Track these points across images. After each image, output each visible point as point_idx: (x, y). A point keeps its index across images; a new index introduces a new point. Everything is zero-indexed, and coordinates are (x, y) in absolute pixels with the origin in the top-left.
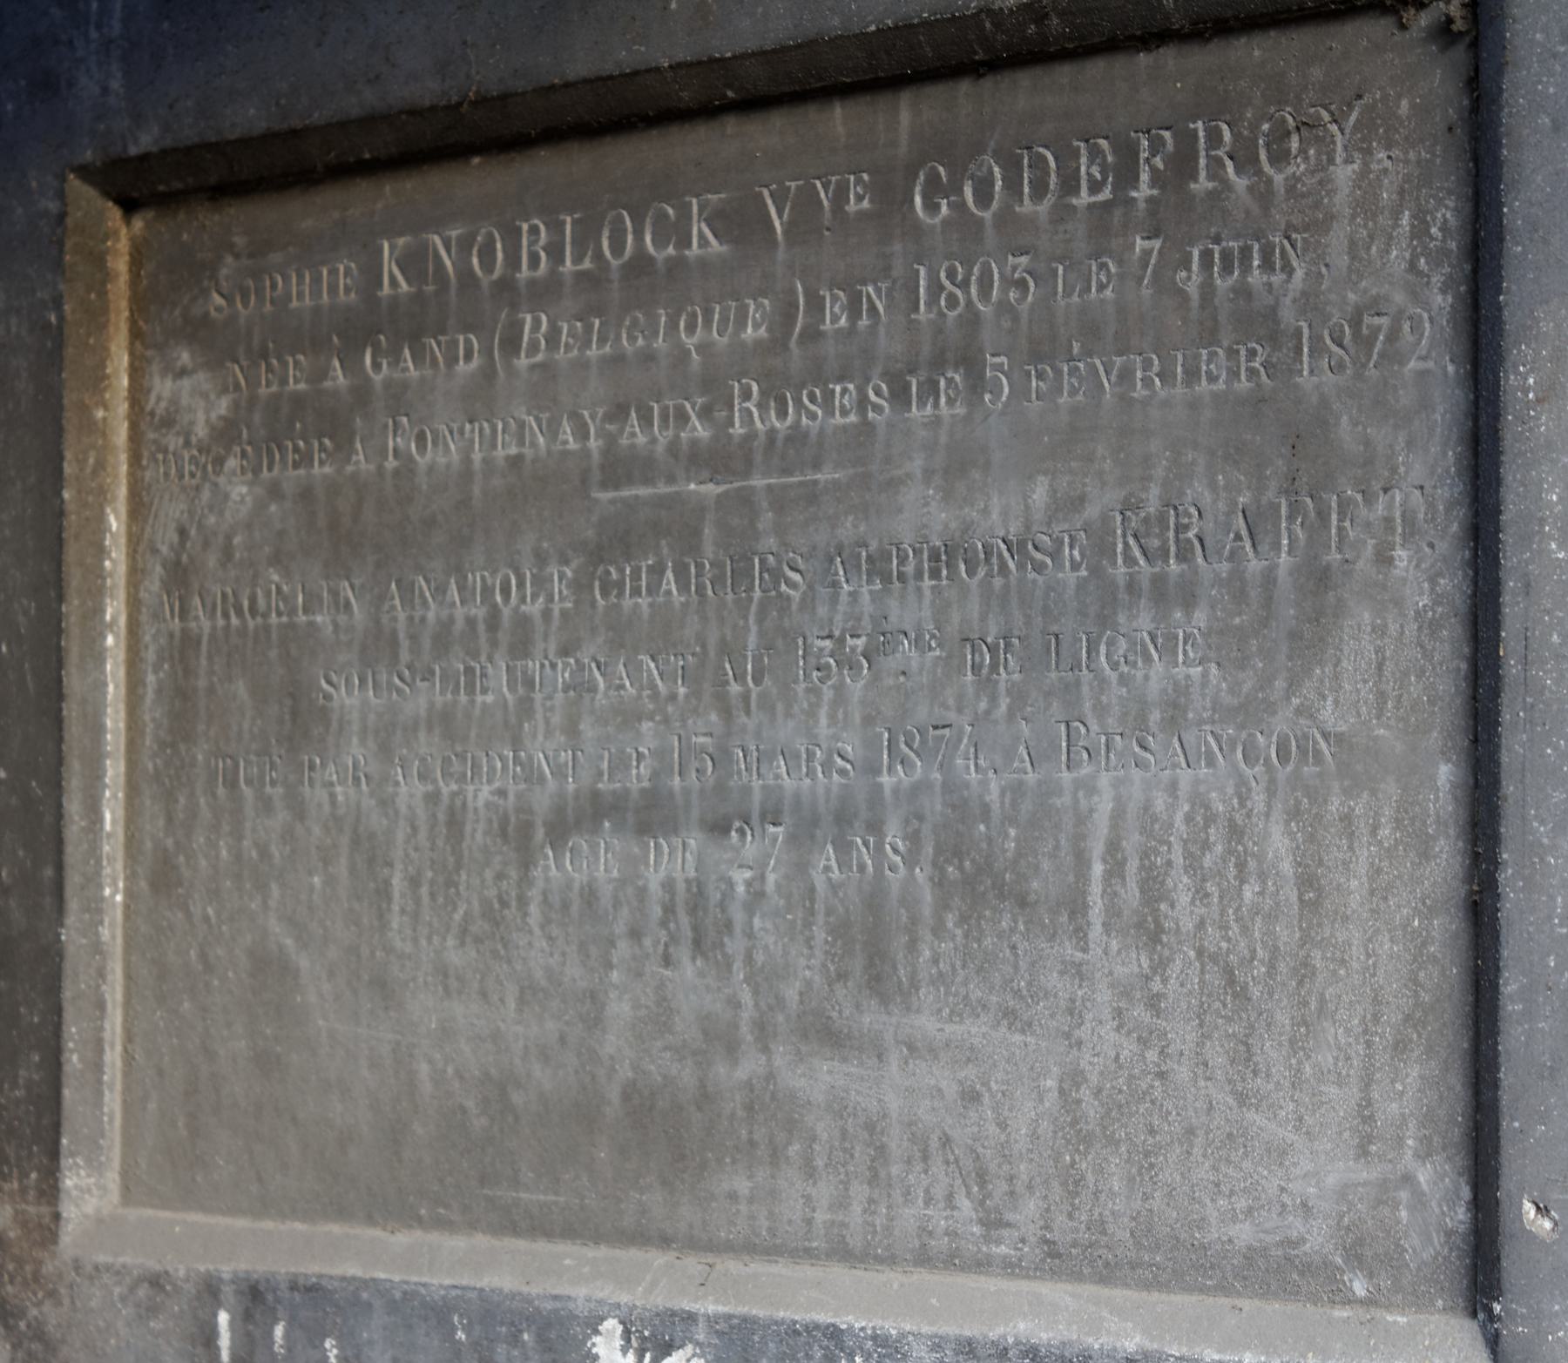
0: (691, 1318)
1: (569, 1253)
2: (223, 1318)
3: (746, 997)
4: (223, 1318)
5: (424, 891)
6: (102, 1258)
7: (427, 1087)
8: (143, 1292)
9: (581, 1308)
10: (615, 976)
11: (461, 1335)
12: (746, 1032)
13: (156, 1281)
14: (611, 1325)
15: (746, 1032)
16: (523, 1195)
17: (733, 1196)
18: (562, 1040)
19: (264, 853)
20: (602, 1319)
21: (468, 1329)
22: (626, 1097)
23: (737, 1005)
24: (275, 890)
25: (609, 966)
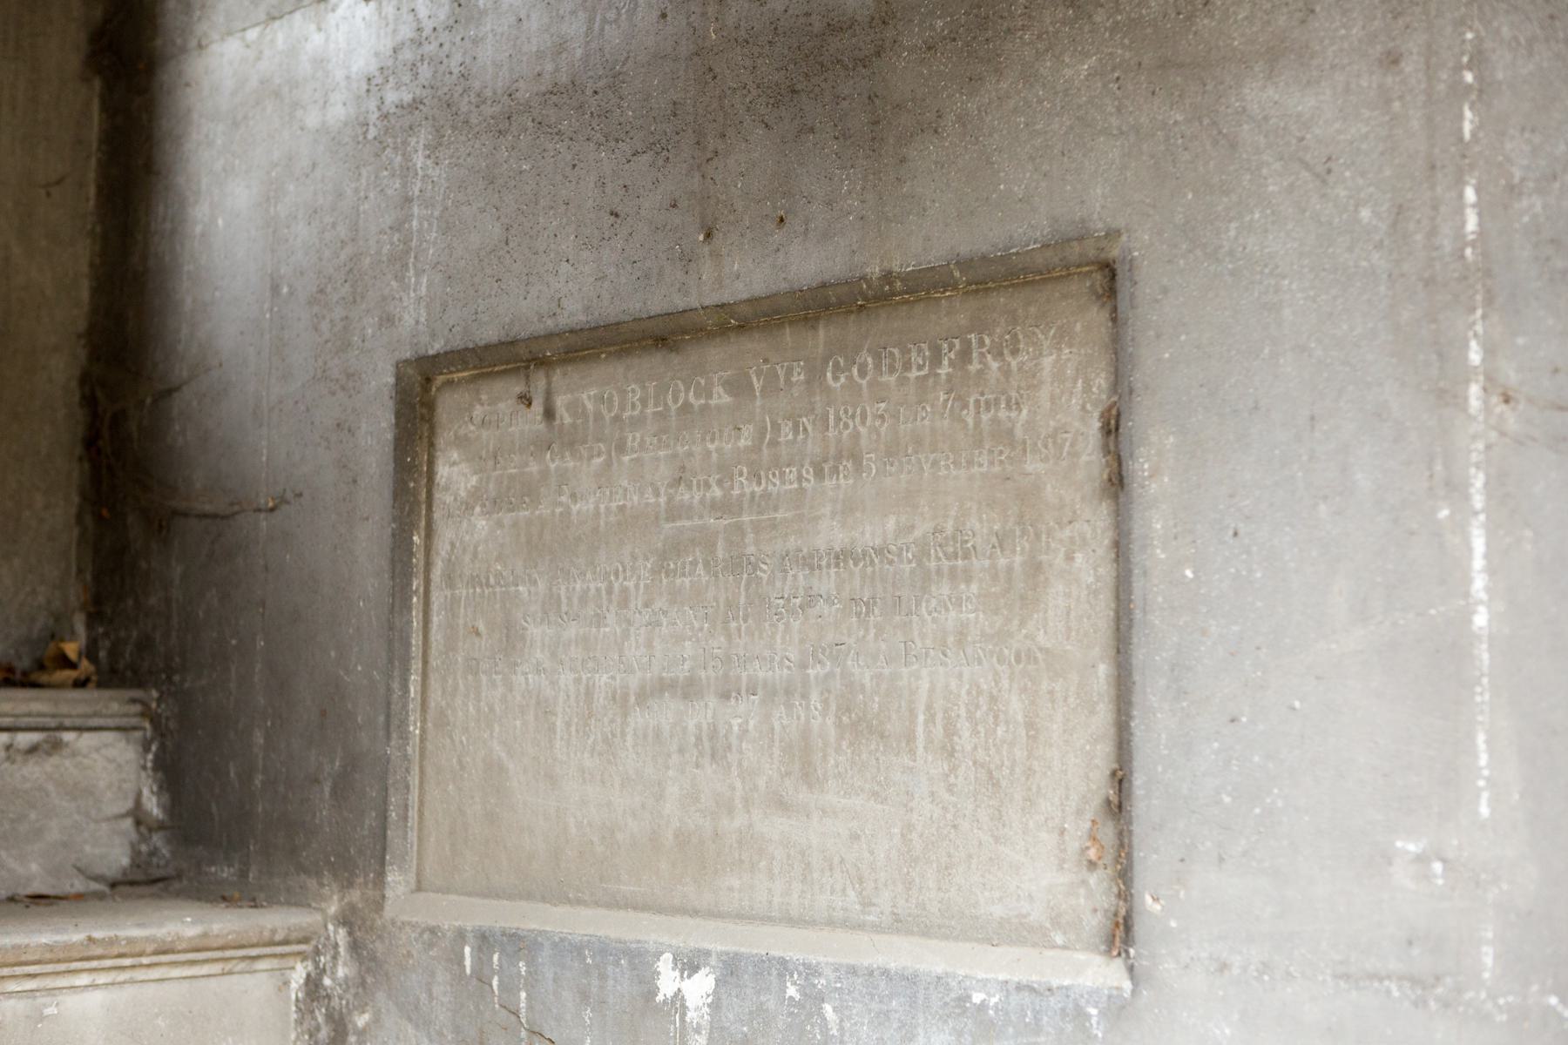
0: (708, 953)
1: (645, 918)
2: (467, 950)
3: (738, 784)
4: (467, 950)
5: (573, 729)
6: (405, 918)
7: (573, 830)
8: (426, 936)
9: (651, 947)
10: (671, 773)
11: (589, 961)
12: (738, 803)
13: (433, 931)
14: (668, 957)
15: (738, 803)
16: (623, 888)
17: (731, 889)
18: (643, 806)
19: (491, 709)
20: (662, 953)
21: (593, 957)
22: (676, 836)
23: (733, 789)
24: (497, 729)
25: (668, 768)
